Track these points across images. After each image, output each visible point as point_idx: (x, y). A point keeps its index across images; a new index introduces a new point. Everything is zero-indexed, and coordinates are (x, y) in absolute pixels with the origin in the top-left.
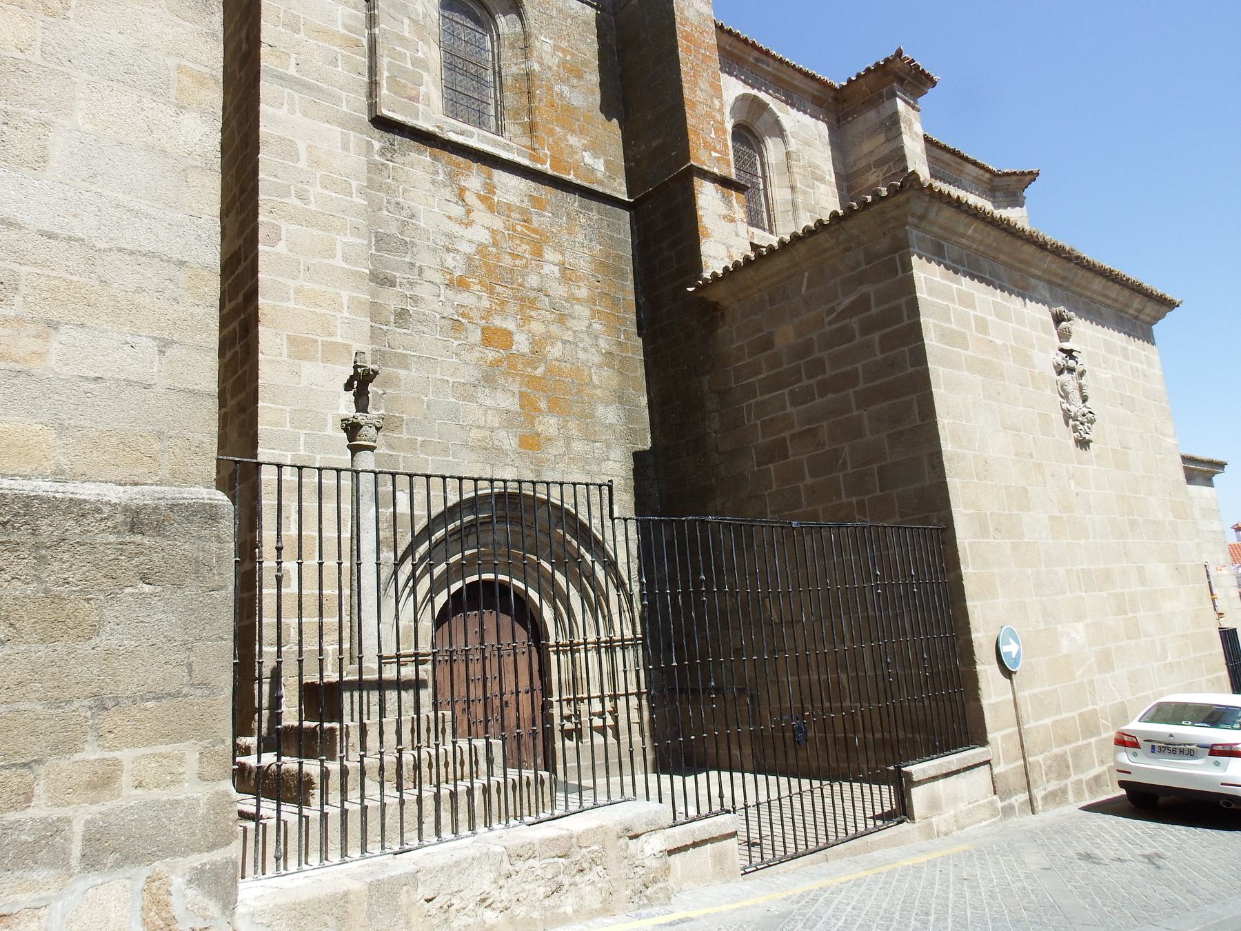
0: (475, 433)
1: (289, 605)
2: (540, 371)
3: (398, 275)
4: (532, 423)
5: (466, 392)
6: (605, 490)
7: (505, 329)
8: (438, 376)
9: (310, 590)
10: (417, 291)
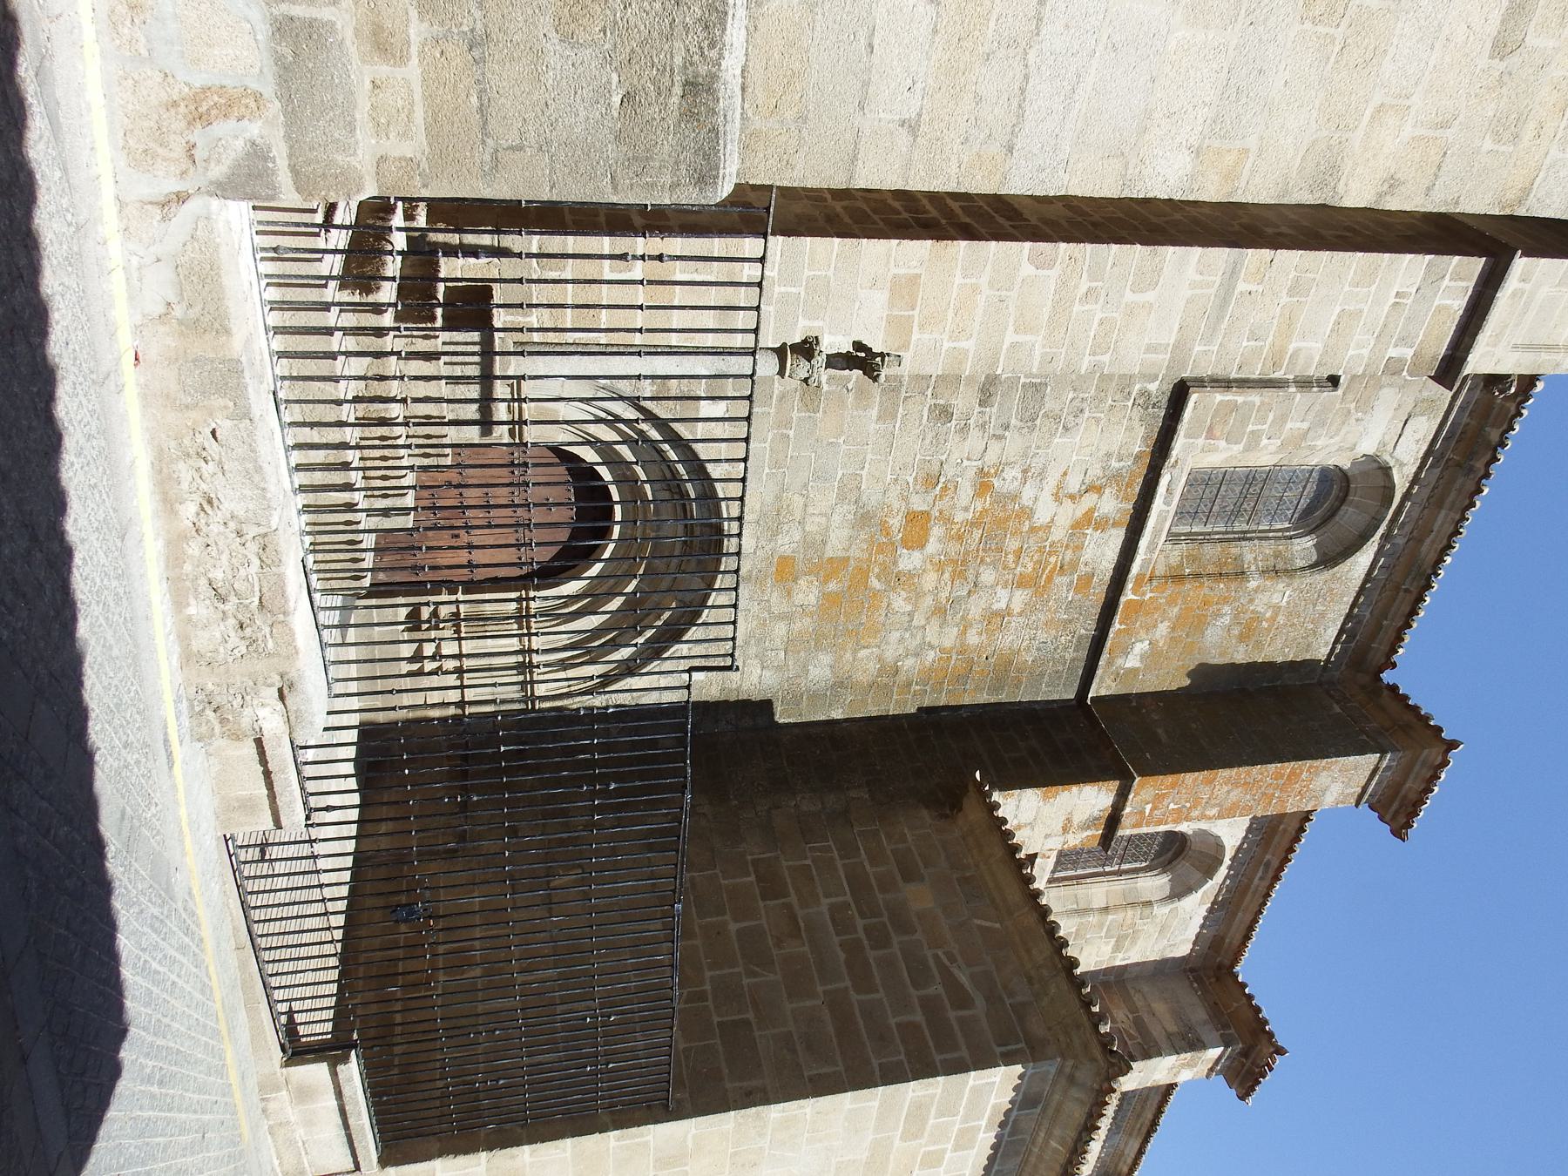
0: (798, 501)
2: (875, 583)
3: (994, 410)
5: (849, 490)
6: (728, 662)
8: (869, 456)
10: (974, 433)
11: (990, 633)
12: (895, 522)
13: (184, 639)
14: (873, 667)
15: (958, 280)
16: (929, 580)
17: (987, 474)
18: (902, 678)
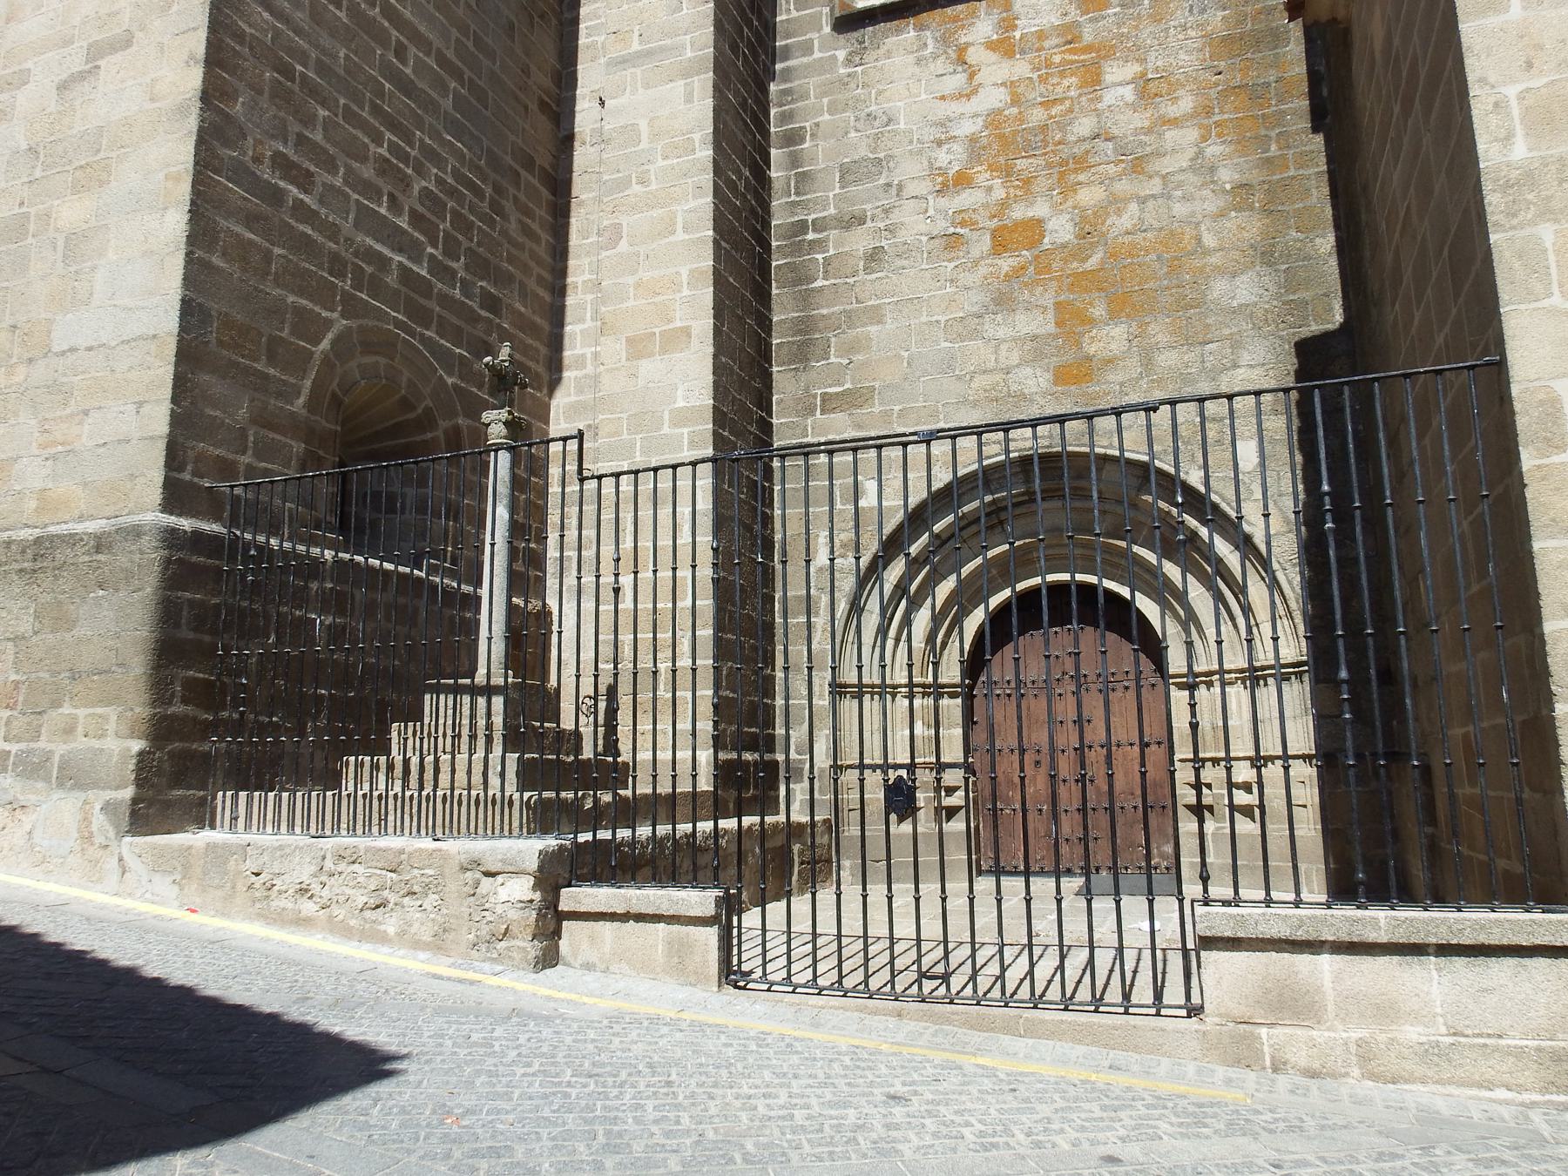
0: (980, 382)
1: (625, 621)
2: (1093, 262)
3: (868, 206)
4: (1079, 345)
5: (967, 328)
6: (573, 446)
7: (1032, 219)
8: (924, 319)
9: (645, 605)
10: (895, 217)
11: (1173, 87)
12: (1006, 264)
13: (417, 945)
14: (1234, 220)
15: (631, 303)
16: (1089, 196)
17: (944, 184)
18: (1255, 176)
